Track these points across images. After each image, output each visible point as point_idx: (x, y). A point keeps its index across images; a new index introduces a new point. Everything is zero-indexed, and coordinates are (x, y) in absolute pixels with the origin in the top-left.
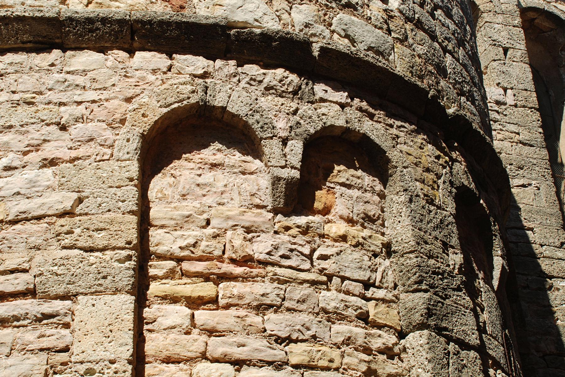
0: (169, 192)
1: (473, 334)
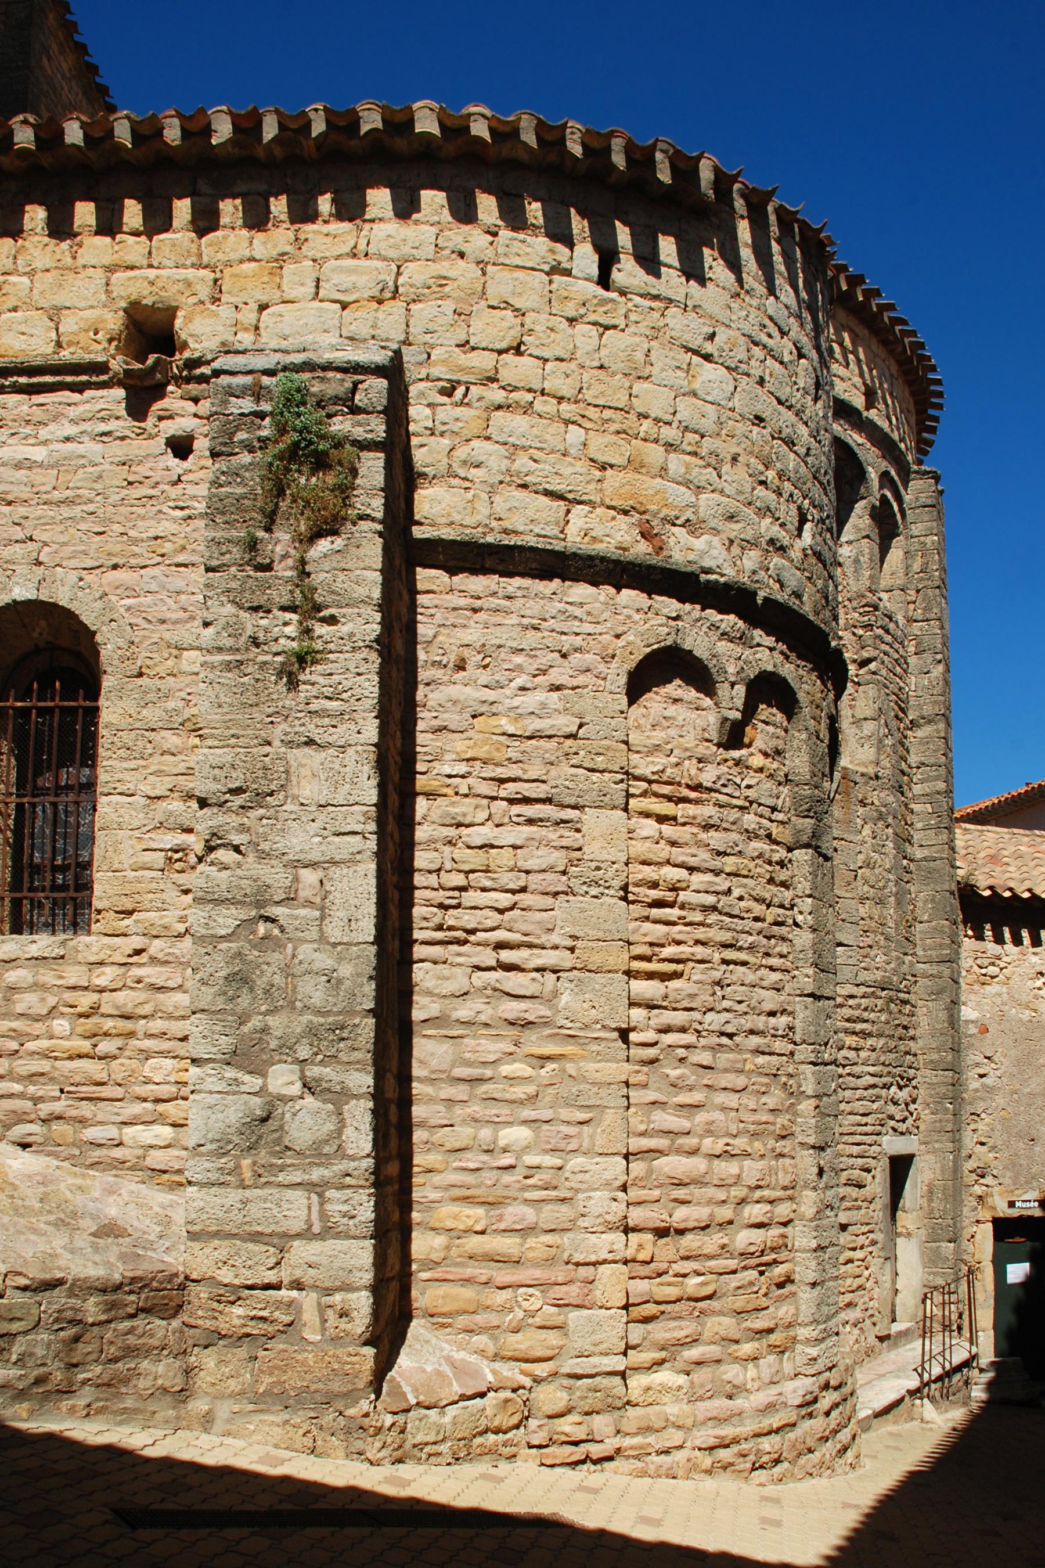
0: (642, 721)
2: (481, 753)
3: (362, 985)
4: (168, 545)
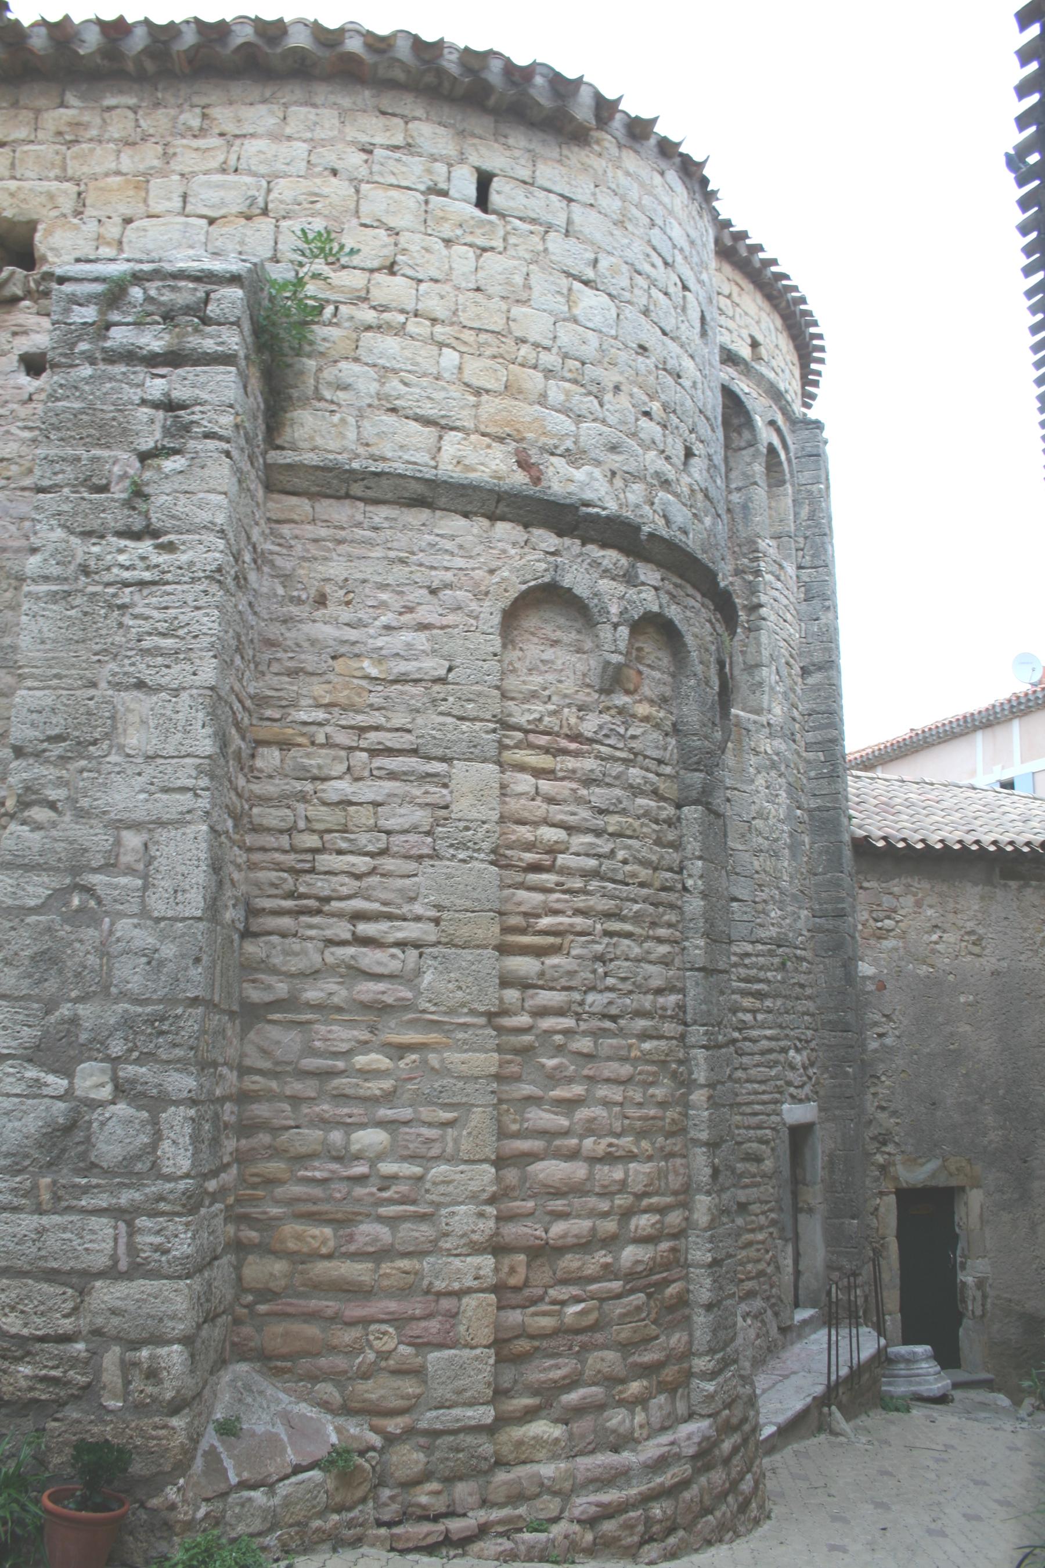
2: (342, 697)
3: (186, 969)
4: (14, 468)
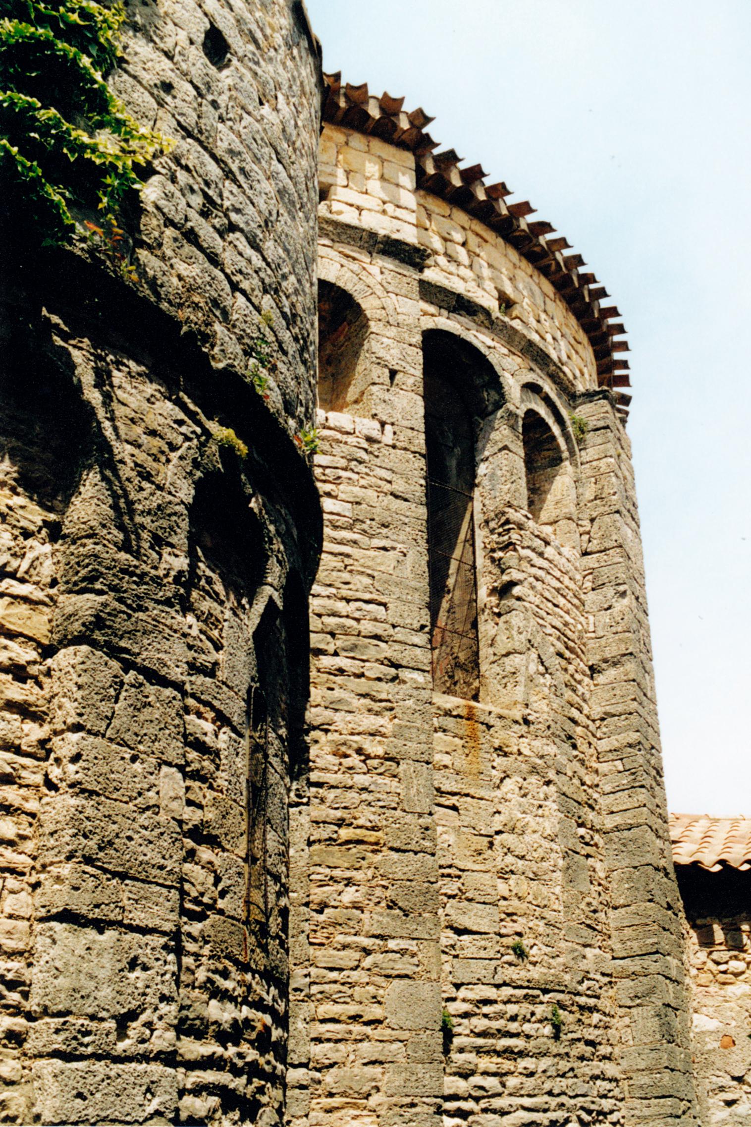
1: (177, 666)
